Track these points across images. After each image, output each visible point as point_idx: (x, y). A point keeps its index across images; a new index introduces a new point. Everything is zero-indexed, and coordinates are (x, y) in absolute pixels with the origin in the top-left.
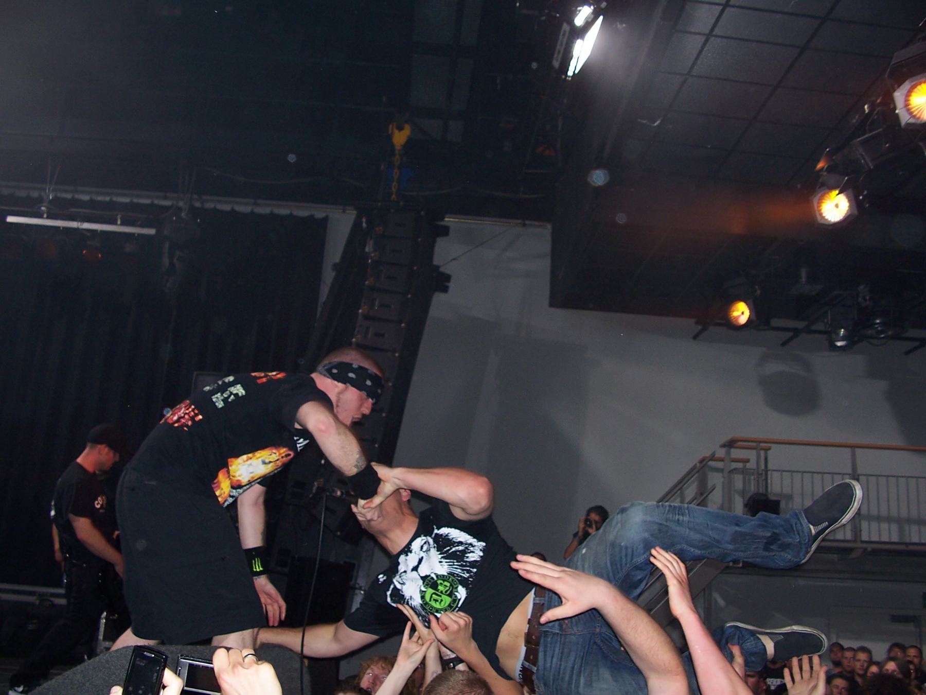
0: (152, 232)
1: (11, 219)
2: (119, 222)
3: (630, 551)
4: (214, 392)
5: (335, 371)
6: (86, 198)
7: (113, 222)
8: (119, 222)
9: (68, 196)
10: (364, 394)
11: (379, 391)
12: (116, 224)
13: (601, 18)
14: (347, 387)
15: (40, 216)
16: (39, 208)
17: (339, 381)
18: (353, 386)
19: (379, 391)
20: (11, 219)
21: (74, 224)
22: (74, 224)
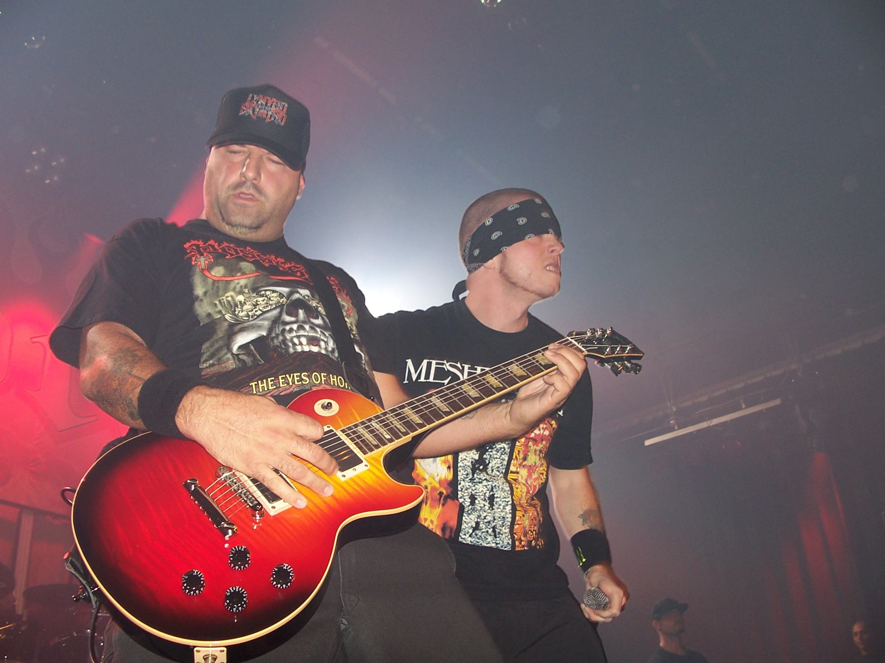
0: (777, 402)
1: (647, 443)
2: (744, 406)
3: (357, 480)
4: (294, 349)
5: (476, 252)
6: (704, 399)
7: (737, 408)
8: (744, 406)
9: (689, 403)
10: (531, 239)
11: (545, 215)
12: (741, 409)
13: (213, 149)
14: (505, 256)
15: (672, 430)
16: (669, 422)
17: (491, 258)
18: (509, 244)
19: (545, 215)
20: (647, 443)
21: (704, 425)
22: (704, 425)
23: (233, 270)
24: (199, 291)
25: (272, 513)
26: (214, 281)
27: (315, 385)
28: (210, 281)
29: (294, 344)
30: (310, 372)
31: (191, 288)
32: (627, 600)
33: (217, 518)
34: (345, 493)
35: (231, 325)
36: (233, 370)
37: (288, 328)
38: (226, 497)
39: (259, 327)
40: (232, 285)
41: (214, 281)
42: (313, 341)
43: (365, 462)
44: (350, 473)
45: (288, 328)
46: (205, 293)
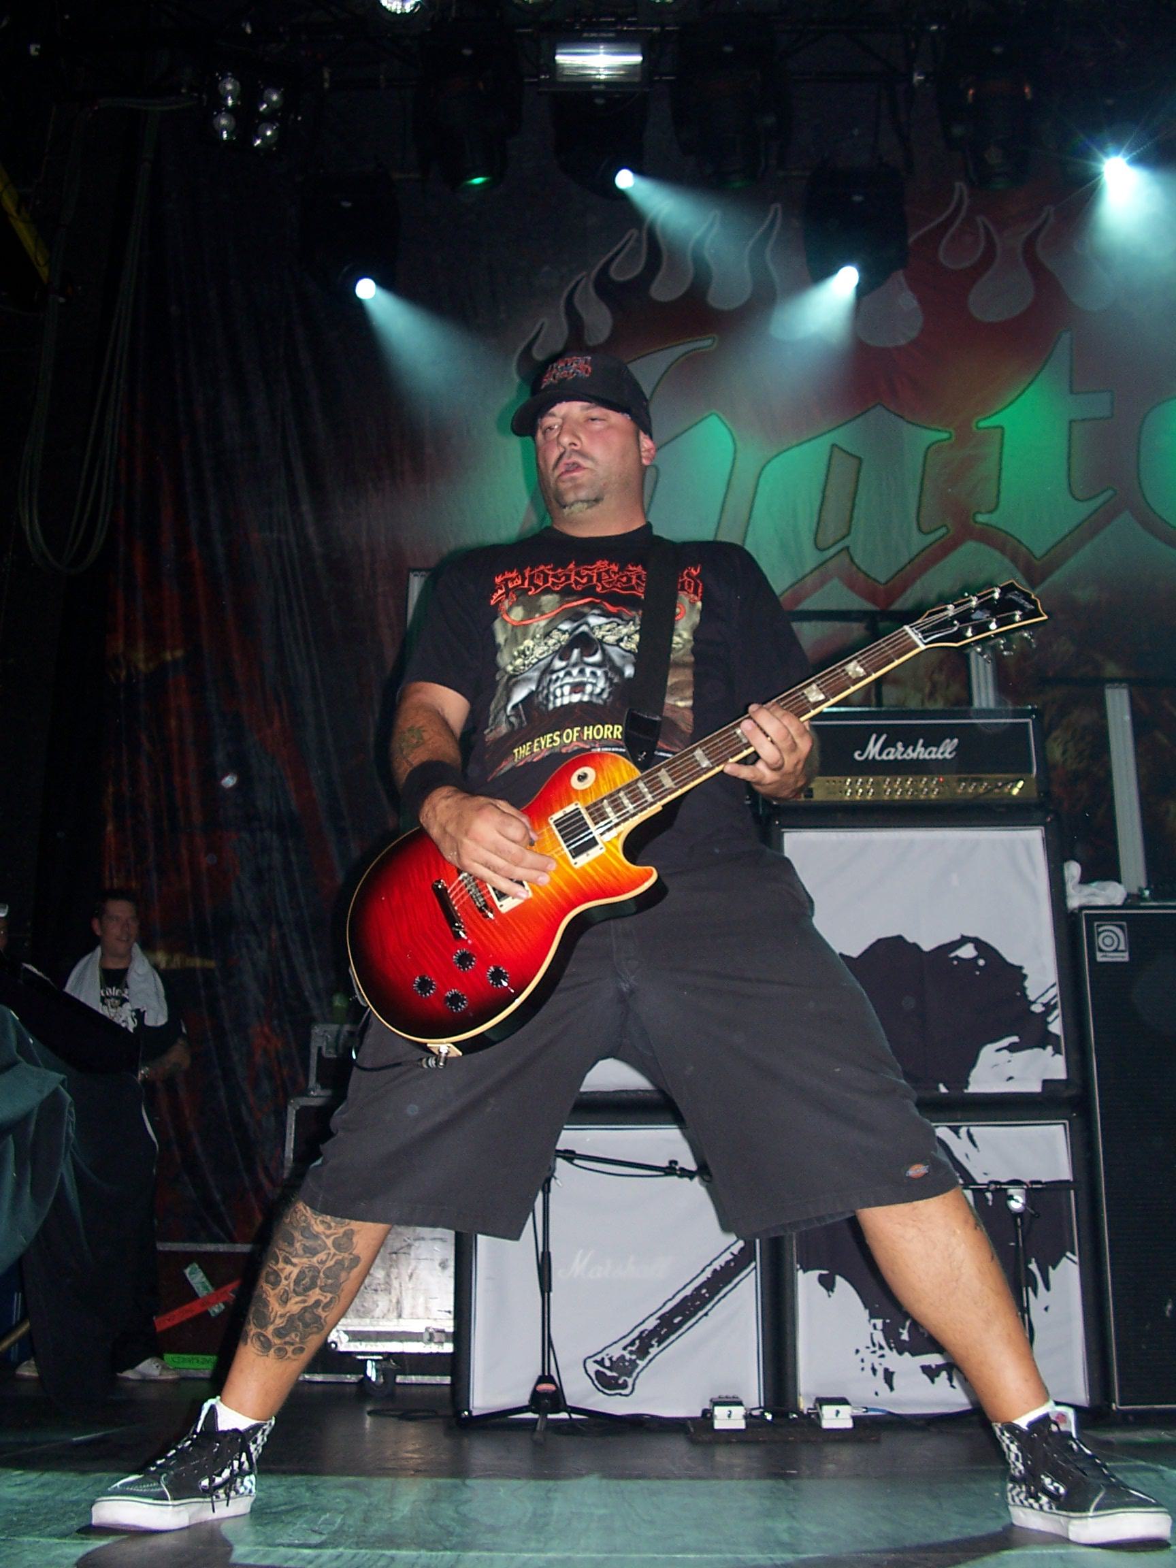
23: (532, 609)
24: (500, 638)
25: (504, 910)
26: (514, 626)
27: (565, 745)
28: (510, 626)
29: (556, 697)
30: (562, 729)
31: (493, 636)
32: (678, 1119)
33: (451, 918)
34: (611, 878)
35: (511, 677)
36: (695, 675)
37: (554, 677)
38: (461, 890)
39: (529, 680)
40: (532, 629)
41: (514, 626)
42: (578, 687)
43: (601, 845)
44: (583, 860)
45: (554, 677)
46: (506, 640)
